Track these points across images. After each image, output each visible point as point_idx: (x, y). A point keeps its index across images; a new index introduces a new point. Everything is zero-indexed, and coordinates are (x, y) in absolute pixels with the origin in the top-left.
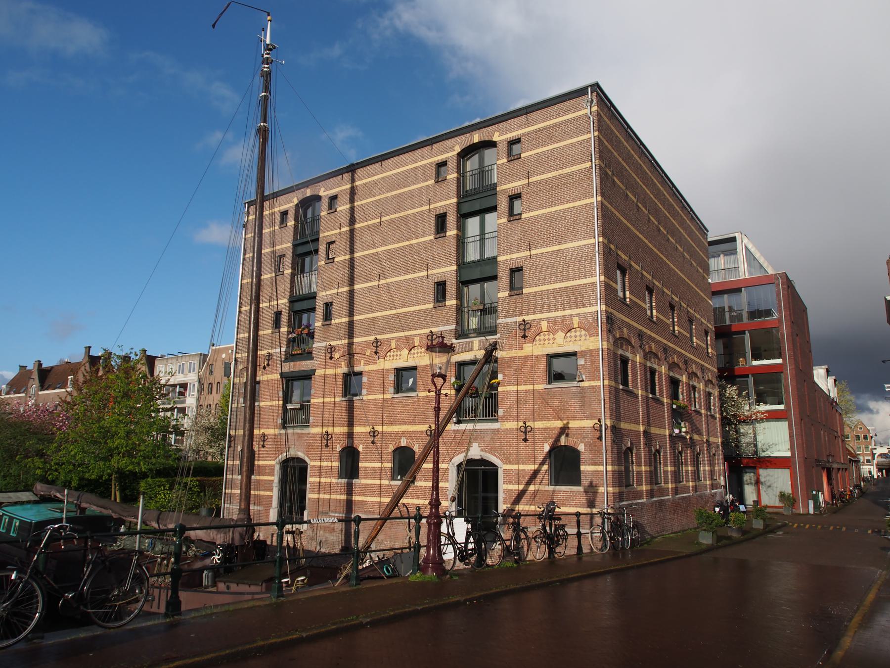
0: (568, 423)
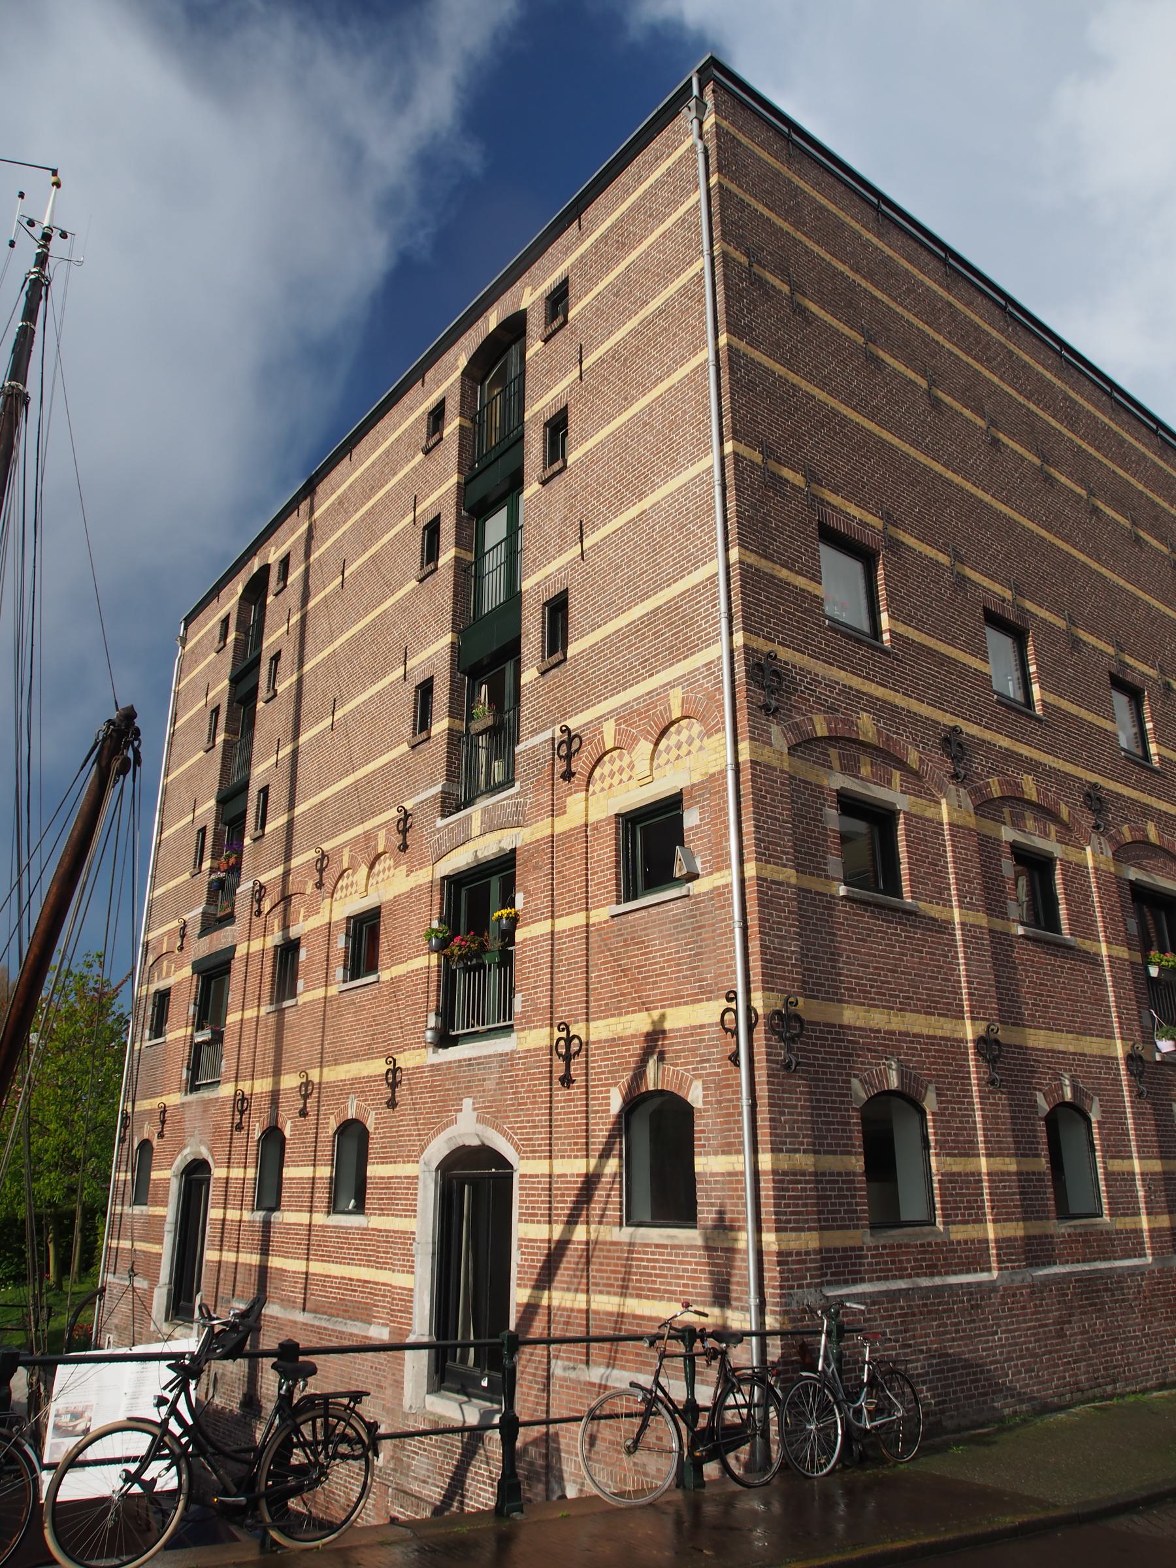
0: (663, 1017)
